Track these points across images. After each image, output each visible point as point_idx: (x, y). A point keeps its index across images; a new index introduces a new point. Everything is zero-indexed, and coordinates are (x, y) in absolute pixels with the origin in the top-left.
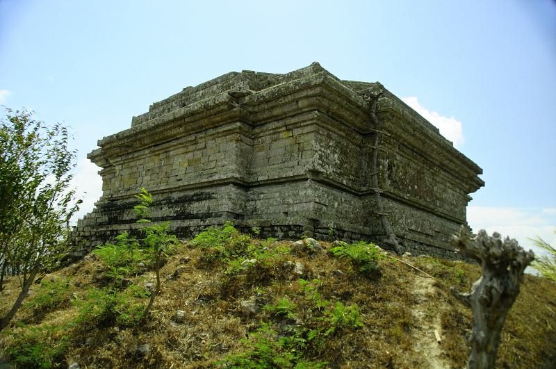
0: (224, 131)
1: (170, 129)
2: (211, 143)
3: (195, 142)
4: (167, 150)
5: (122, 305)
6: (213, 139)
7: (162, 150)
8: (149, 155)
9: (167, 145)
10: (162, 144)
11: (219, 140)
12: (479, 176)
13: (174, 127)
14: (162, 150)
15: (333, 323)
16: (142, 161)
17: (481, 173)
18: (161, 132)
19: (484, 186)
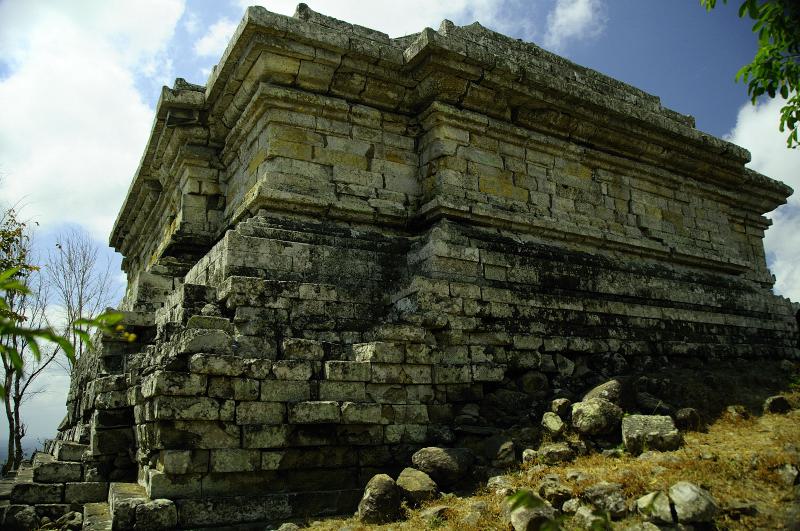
0: (724, 196)
1: (649, 141)
2: (696, 201)
3: (675, 186)
4: (620, 170)
5: (733, 443)
6: (702, 197)
7: (612, 164)
8: (572, 156)
9: (626, 162)
10: (624, 156)
11: (709, 203)
12: (747, 165)
13: (658, 143)
14: (612, 164)
15: (146, 468)
16: (546, 159)
17: (748, 161)
18: (631, 134)
19: (771, 224)
